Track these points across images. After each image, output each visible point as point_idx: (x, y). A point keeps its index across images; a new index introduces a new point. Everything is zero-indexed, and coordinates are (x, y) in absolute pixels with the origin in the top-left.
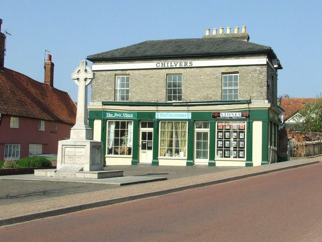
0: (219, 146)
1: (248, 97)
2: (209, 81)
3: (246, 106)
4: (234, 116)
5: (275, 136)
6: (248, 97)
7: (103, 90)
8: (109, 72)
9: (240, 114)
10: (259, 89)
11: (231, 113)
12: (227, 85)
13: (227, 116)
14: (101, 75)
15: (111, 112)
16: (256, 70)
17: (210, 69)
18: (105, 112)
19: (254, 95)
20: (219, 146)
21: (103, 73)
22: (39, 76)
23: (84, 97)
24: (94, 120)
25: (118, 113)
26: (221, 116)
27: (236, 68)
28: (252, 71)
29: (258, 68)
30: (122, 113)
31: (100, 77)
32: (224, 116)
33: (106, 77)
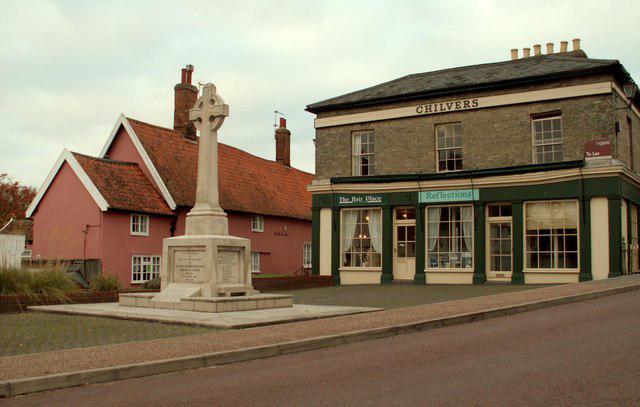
21: (333, 131)
29: (597, 102)
30: (363, 196)
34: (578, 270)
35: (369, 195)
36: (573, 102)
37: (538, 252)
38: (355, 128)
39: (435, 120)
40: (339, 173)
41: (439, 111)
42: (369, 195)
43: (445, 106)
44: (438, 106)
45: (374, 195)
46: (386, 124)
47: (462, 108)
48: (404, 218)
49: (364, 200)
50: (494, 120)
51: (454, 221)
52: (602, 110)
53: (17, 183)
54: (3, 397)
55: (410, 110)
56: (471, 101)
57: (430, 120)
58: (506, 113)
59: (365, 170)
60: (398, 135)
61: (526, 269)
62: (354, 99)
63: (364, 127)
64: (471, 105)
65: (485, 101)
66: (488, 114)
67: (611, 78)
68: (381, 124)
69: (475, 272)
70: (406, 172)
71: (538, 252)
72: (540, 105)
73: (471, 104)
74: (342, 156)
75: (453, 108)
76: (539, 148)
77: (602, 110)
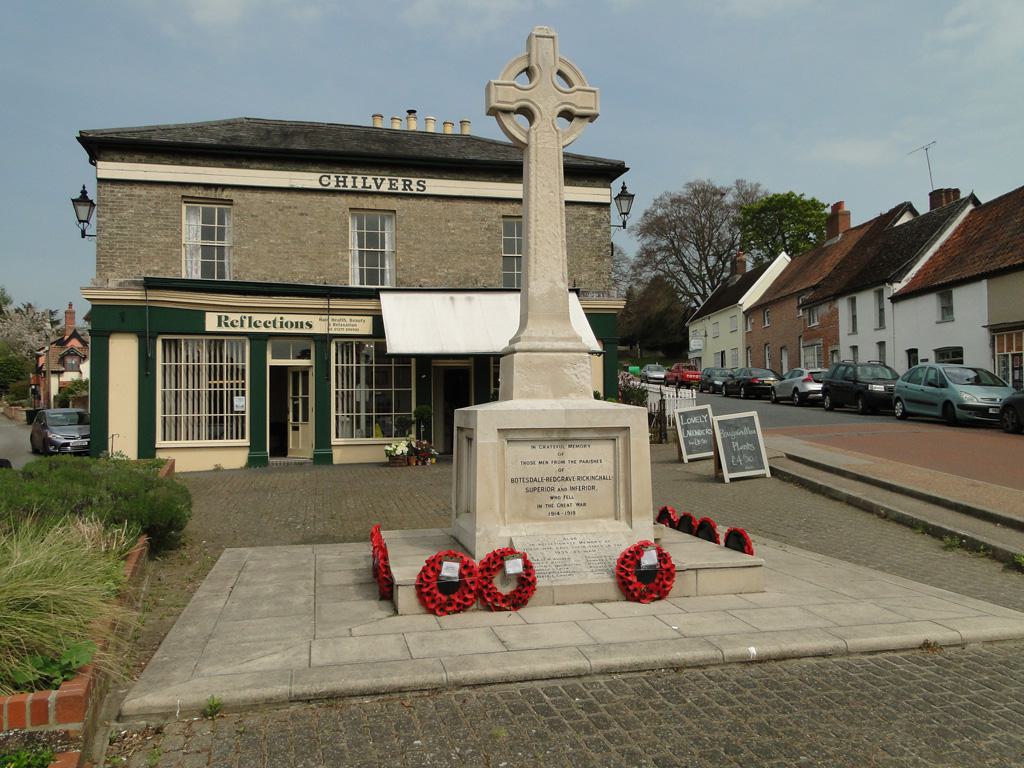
7: (141, 242)
10: (593, 262)
17: (471, 205)
21: (138, 191)
29: (591, 212)
33: (151, 203)
34: (246, 442)
38: (192, 192)
39: (352, 201)
40: (157, 270)
41: (349, 188)
43: (370, 181)
44: (355, 181)
46: (258, 195)
47: (400, 191)
51: (174, 363)
53: (758, 185)
54: (82, 759)
55: (309, 179)
56: (414, 181)
57: (342, 200)
58: (468, 209)
59: (206, 268)
60: (281, 217)
61: (159, 443)
62: (156, 138)
63: (211, 194)
64: (400, 187)
65: (436, 186)
66: (439, 205)
68: (248, 195)
69: (250, 447)
70: (296, 281)
71: (374, 414)
73: (414, 187)
74: (161, 238)
75: (385, 188)
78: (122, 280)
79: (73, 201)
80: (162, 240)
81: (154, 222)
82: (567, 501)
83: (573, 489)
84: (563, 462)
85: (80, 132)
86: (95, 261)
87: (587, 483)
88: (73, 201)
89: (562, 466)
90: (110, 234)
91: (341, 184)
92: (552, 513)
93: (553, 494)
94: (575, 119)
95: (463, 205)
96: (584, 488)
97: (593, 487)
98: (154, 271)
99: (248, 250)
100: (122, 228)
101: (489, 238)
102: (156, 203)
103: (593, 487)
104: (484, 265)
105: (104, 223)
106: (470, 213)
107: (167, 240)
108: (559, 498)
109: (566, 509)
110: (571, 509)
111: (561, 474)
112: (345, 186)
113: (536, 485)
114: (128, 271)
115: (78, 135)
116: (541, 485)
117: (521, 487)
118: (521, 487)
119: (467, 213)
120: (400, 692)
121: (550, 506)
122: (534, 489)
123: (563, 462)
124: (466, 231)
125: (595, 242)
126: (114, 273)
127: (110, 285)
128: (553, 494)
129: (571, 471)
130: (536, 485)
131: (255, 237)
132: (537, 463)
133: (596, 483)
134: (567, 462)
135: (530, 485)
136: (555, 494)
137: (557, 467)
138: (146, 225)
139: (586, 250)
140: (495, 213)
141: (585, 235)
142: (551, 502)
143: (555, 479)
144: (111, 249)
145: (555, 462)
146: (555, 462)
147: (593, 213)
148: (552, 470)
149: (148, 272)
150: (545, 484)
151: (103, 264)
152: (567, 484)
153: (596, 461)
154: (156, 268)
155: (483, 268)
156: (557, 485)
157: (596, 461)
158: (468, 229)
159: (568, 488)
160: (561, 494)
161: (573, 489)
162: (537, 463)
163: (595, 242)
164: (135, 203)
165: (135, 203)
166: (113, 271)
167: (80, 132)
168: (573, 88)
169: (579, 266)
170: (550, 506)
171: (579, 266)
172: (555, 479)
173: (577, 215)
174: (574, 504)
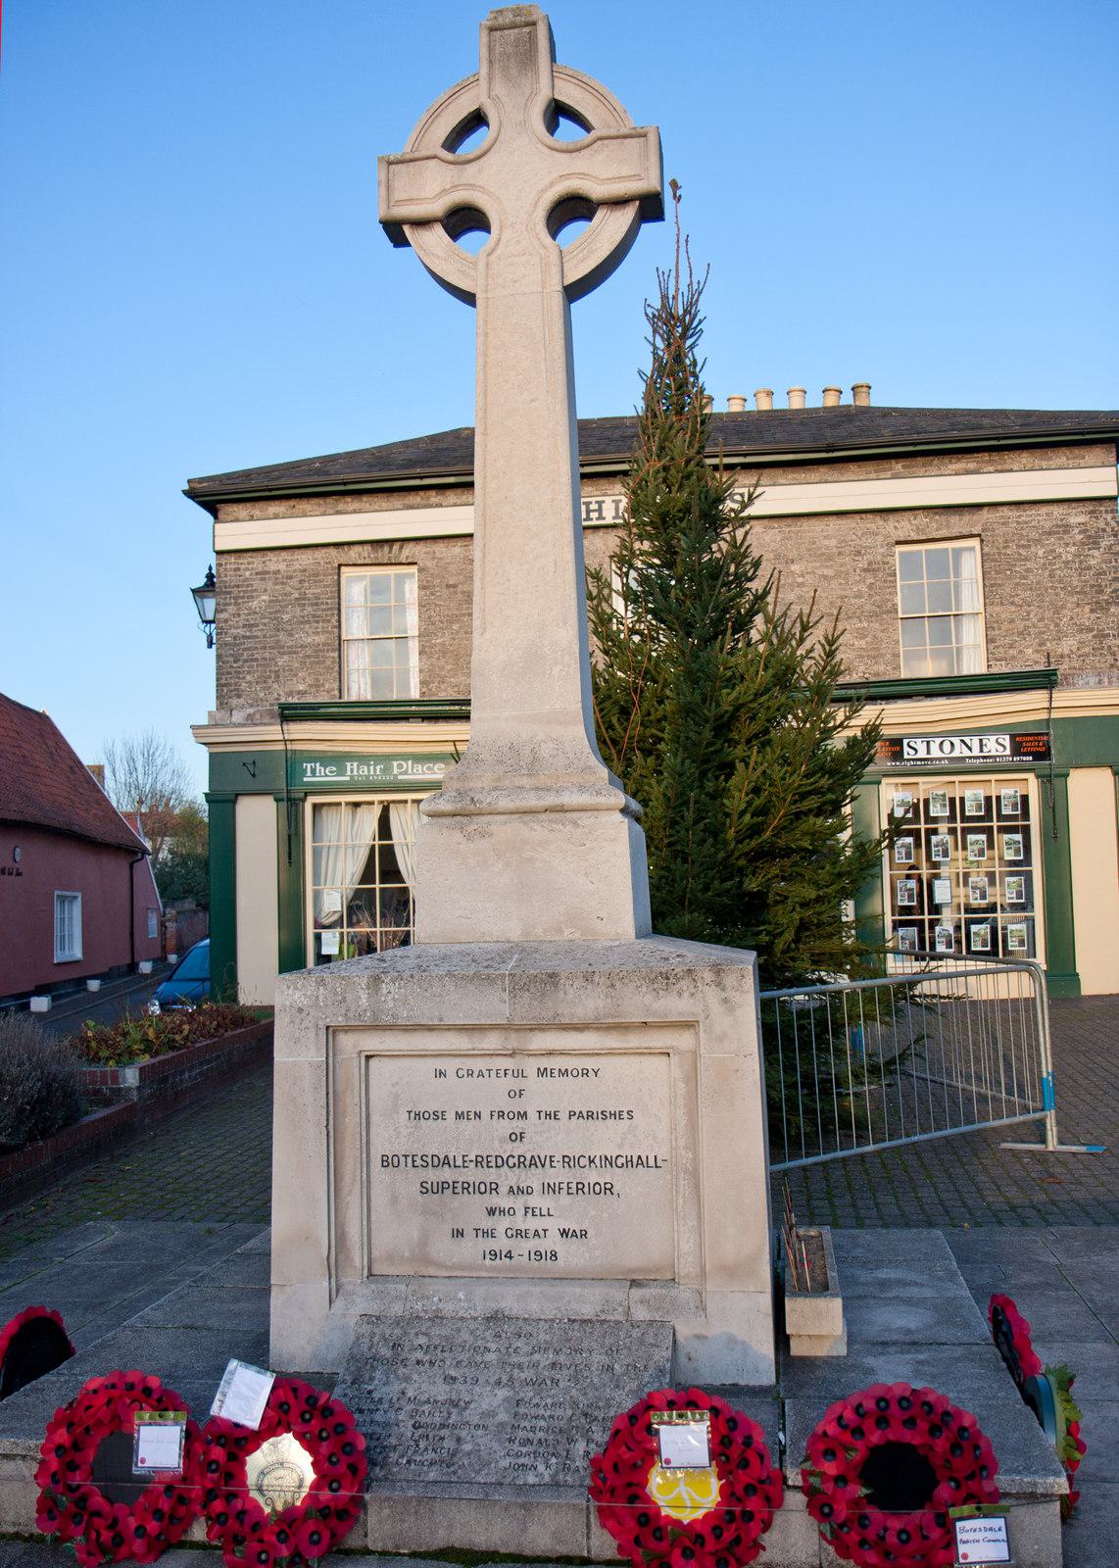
0: (967, 814)
1: (1036, 656)
2: (834, 584)
3: (1036, 699)
4: (976, 752)
5: (1045, 1039)
6: (1036, 656)
7: (278, 646)
8: (305, 559)
9: (1006, 740)
10: (1086, 617)
11: (956, 741)
12: (112, 1077)
13: (935, 753)
14: (263, 574)
15: (326, 759)
16: (1067, 528)
17: (833, 522)
18: (292, 762)
19: (1068, 645)
20: (967, 814)
21: (275, 563)
22: (635, 414)
23: (773, 470)
24: (234, 802)
25: (362, 759)
26: (907, 753)
27: (966, 518)
28: (1050, 533)
29: (1077, 517)
30: (386, 759)
31: (257, 584)
32: (923, 753)
33: (294, 582)
35: (404, 757)
36: (1011, 513)
37: (378, 929)
38: (354, 553)
40: (299, 689)
42: (404, 757)
45: (419, 758)
48: (941, 957)
49: (387, 770)
50: (945, 1164)
52: (1092, 540)
67: (647, 1490)
68: (439, 548)
71: (378, 886)
72: (922, 519)
74: (311, 637)
76: (925, 790)
77: (1092, 540)
78: (251, 711)
79: (193, 591)
80: (310, 640)
81: (298, 611)
82: (533, 1224)
83: (551, 1189)
84: (524, 1115)
85: (189, 481)
86: (215, 683)
87: (592, 1176)
88: (193, 591)
89: (518, 1125)
90: (235, 638)
91: (594, 515)
92: (494, 1255)
93: (495, 1201)
94: (600, 214)
95: (818, 525)
96: (580, 1187)
97: (609, 1189)
98: (299, 692)
99: (443, 644)
100: (251, 626)
101: (871, 586)
102: (301, 582)
103: (609, 1189)
104: (865, 637)
105: (226, 621)
106: (833, 542)
107: (317, 638)
108: (511, 1211)
109: (532, 1244)
110: (545, 1245)
111: (518, 1149)
112: (600, 517)
113: (446, 1174)
114: (262, 695)
115: (186, 487)
116: (462, 1176)
117: (409, 1182)
118: (409, 1182)
119: (826, 542)
120: (914, 1343)
121: (485, 1233)
122: (443, 1187)
123: (524, 1115)
124: (825, 577)
125: (1089, 575)
126: (241, 701)
127: (234, 719)
128: (495, 1201)
129: (543, 1139)
130: (446, 1174)
131: (452, 622)
132: (450, 1116)
133: (617, 1177)
134: (532, 1115)
135: (433, 1176)
136: (502, 1201)
137: (506, 1126)
138: (286, 617)
139: (1071, 594)
140: (880, 539)
141: (1067, 562)
142: (487, 1223)
143: (502, 1162)
144: (235, 662)
145: (501, 1114)
146: (501, 1114)
147: (1082, 519)
148: (492, 1138)
149: (290, 694)
150: (472, 1175)
151: (227, 690)
152: (534, 1178)
153: (617, 1115)
154: (301, 687)
155: (862, 643)
156: (508, 1177)
157: (617, 1115)
158: (829, 572)
159: (537, 1187)
160: (518, 1201)
161: (551, 1189)
162: (450, 1116)
163: (1089, 575)
164: (270, 585)
165: (270, 585)
166: (239, 696)
167: (189, 481)
168: (593, 134)
169: (1057, 625)
170: (485, 1233)
171: (1057, 625)
172: (502, 1162)
173: (1048, 525)
174: (553, 1233)
